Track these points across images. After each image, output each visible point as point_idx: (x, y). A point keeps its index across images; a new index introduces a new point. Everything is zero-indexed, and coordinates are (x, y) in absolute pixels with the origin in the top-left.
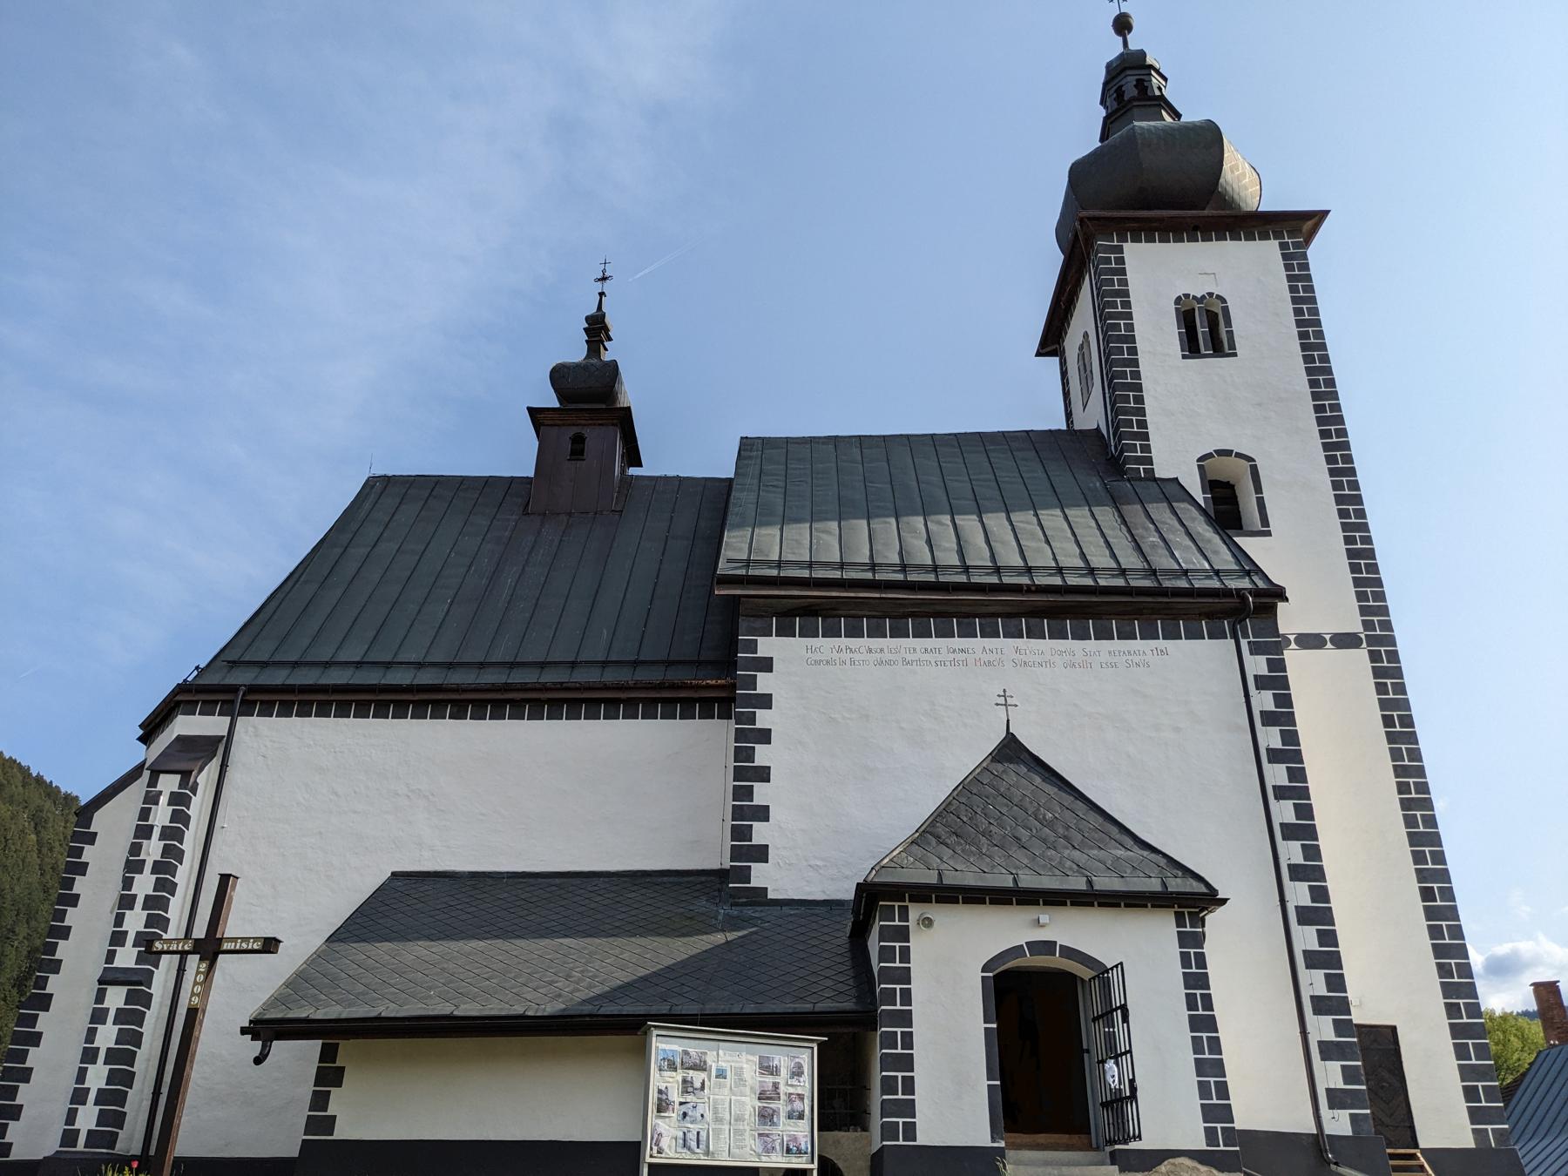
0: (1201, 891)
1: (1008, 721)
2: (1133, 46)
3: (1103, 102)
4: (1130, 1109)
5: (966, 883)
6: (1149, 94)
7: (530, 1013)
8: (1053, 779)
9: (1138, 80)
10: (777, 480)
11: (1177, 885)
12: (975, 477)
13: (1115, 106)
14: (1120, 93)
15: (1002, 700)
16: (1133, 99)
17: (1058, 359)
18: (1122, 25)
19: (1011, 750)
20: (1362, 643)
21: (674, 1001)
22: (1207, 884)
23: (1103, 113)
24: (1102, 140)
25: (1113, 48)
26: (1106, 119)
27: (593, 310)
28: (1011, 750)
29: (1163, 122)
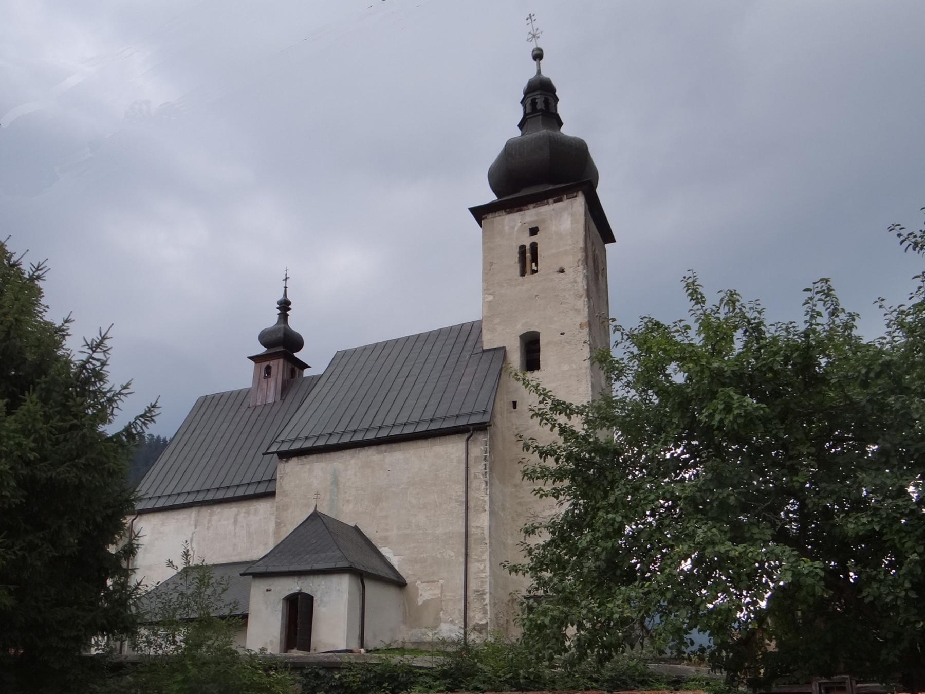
2: (545, 74)
18: (538, 56)
27: (541, 62)
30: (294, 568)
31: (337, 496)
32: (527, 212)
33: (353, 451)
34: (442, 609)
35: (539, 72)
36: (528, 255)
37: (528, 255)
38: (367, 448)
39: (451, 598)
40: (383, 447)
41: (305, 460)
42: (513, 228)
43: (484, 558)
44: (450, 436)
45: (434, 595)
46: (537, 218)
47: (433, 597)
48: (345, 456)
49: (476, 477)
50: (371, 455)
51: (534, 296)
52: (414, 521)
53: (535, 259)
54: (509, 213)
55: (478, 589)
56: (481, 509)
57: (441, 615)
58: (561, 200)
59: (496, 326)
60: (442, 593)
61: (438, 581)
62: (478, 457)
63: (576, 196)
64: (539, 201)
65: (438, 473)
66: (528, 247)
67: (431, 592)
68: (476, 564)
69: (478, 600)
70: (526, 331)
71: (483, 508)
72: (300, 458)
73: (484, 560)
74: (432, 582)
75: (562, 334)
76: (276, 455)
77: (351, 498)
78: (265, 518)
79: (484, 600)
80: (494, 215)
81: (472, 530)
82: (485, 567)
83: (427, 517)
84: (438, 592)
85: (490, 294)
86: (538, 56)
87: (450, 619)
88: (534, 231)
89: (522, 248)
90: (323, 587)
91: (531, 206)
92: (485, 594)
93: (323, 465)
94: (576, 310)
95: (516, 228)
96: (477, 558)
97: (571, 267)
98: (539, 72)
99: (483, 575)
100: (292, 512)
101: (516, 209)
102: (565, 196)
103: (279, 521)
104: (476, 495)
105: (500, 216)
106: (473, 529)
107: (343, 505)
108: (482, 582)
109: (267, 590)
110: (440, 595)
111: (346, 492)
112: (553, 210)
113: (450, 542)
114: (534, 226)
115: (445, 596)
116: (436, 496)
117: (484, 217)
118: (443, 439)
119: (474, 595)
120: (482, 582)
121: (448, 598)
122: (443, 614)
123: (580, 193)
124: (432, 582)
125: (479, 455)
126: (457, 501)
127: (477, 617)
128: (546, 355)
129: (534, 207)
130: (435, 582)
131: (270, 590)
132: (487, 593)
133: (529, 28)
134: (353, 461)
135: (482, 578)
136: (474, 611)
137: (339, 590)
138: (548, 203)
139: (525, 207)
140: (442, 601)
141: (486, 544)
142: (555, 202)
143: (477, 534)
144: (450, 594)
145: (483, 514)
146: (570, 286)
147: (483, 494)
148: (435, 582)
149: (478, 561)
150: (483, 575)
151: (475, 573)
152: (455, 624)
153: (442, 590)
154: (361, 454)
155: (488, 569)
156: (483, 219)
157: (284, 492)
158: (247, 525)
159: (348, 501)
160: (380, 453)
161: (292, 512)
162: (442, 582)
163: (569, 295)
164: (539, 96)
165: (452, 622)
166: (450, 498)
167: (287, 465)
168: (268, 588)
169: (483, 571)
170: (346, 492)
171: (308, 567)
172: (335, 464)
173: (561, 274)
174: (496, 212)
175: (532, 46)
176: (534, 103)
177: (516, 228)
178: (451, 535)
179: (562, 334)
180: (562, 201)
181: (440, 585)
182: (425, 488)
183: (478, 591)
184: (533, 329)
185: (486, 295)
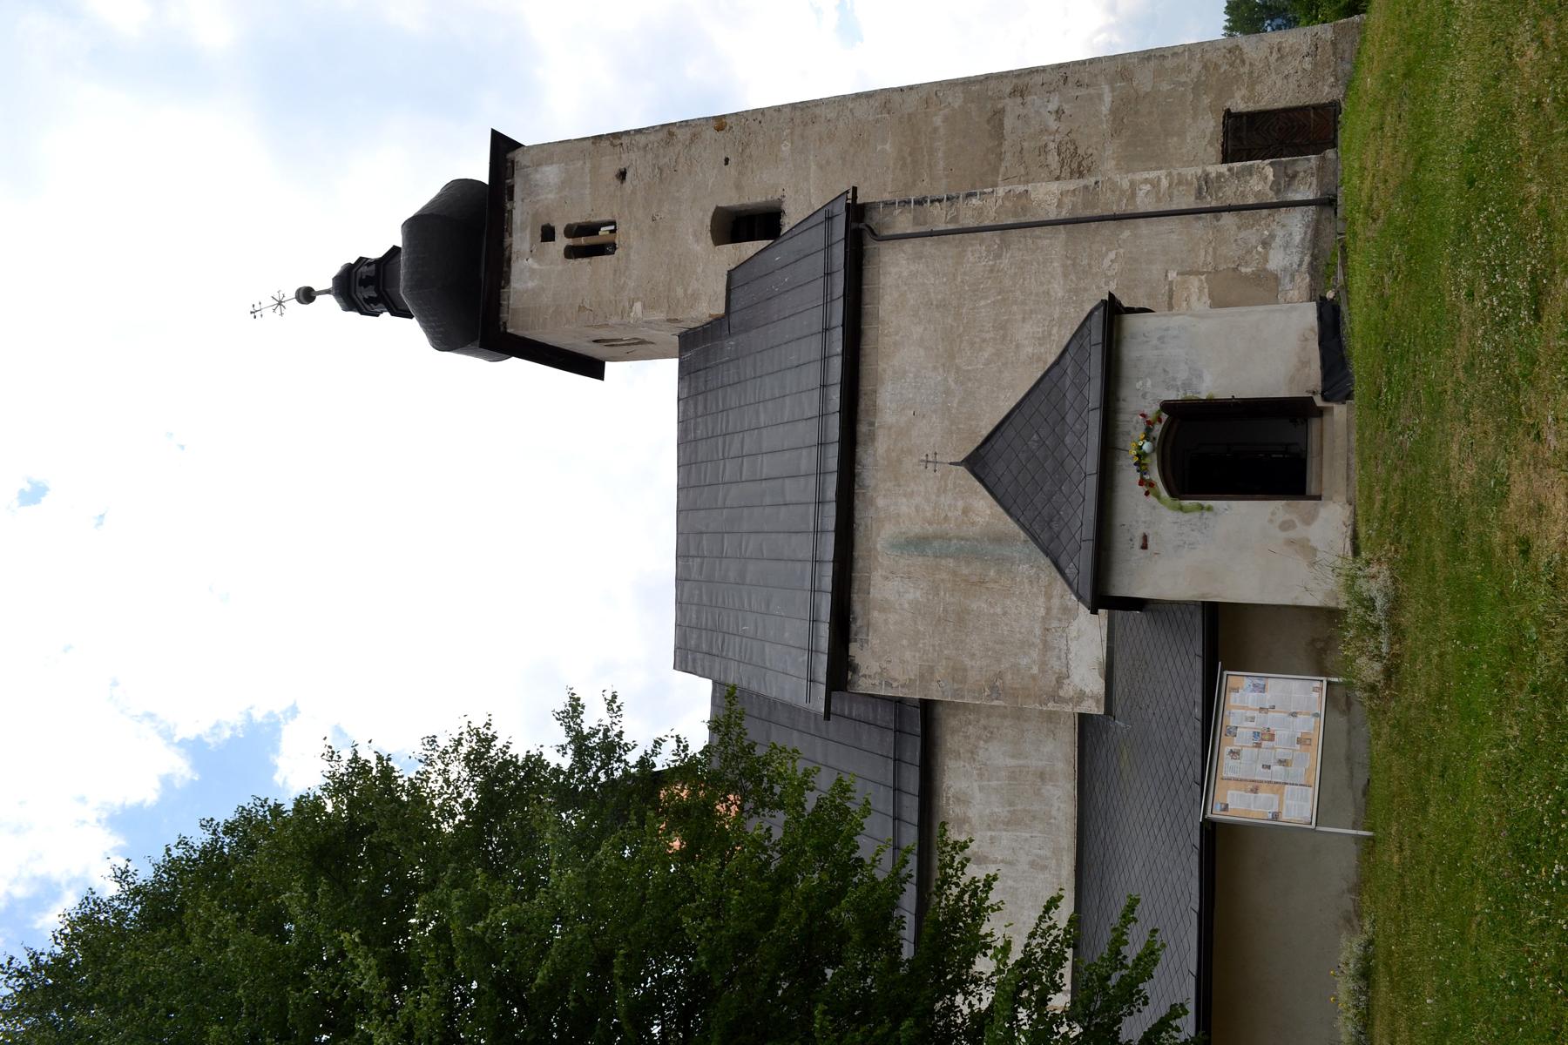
0: (1102, 314)
1: (951, 464)
2: (329, 285)
3: (377, 315)
4: (1314, 424)
5: (1092, 519)
6: (373, 274)
7: (1197, 909)
8: (1002, 430)
9: (360, 285)
10: (717, 640)
11: (1096, 335)
12: (720, 454)
13: (380, 305)
14: (370, 301)
15: (930, 466)
16: (377, 290)
17: (607, 363)
18: (307, 295)
19: (976, 463)
20: (1352, 683)
21: (1191, 779)
22: (1096, 308)
23: (386, 315)
24: (411, 317)
25: (328, 304)
26: (393, 314)
27: (316, 289)
28: (976, 463)
29: (403, 258)
30: (1091, 463)
31: (950, 540)
32: (515, 247)
33: (858, 503)
34: (1235, 270)
35: (327, 292)
36: (583, 241)
37: (583, 241)
38: (858, 469)
39: (1211, 250)
40: (863, 428)
41: (859, 623)
42: (532, 271)
43: (1125, 184)
44: (865, 281)
45: (1201, 290)
46: (529, 229)
47: (1206, 290)
48: (864, 516)
49: (954, 219)
50: (875, 456)
51: (653, 224)
52: (1030, 350)
53: (591, 229)
54: (508, 282)
55: (1193, 192)
56: (1024, 201)
57: (1249, 270)
58: (511, 189)
59: (689, 292)
60: (1198, 273)
61: (1171, 282)
62: (914, 218)
63: (513, 162)
64: (503, 225)
65: (934, 303)
66: (570, 242)
67: (1194, 298)
68: (1138, 200)
69: (1220, 188)
70: (709, 234)
71: (1020, 196)
72: (852, 636)
73: (1132, 184)
74: (1171, 297)
75: (727, 161)
76: (834, 693)
77: (960, 504)
78: (981, 775)
79: (1220, 175)
80: (504, 309)
81: (1064, 214)
82: (1146, 181)
83: (1024, 320)
84: (1194, 282)
85: (631, 307)
86: (307, 295)
87: (1260, 249)
88: (548, 234)
89: (572, 253)
90: (1149, 383)
91: (507, 241)
92: (1207, 175)
93: (877, 577)
94: (692, 141)
95: (536, 266)
96: (1125, 201)
97: (620, 158)
98: (327, 292)
99: (1165, 183)
100: (973, 656)
101: (505, 269)
102: (508, 181)
103: (988, 692)
104: (992, 214)
105: (509, 297)
106: (1064, 213)
107: (973, 524)
108: (1180, 183)
109: (1145, 547)
110: (1203, 277)
111: (946, 517)
112: (523, 200)
113: (1085, 262)
114: (539, 233)
115: (1205, 264)
116: (983, 303)
117: (502, 329)
118: (867, 298)
119: (1209, 198)
120: (1180, 183)
121: (1209, 259)
122: (1247, 264)
123: (510, 156)
124: (1171, 297)
125: (910, 217)
126: (998, 256)
127: (1256, 189)
128: (753, 195)
129: (511, 235)
130: (1171, 290)
131: (1145, 538)
132: (1204, 171)
133: (268, 312)
134: (881, 502)
135: (1170, 185)
136: (1243, 195)
137: (1161, 339)
138: (511, 212)
139: (507, 253)
140: (1216, 271)
141: (1096, 183)
142: (511, 199)
143: (1074, 206)
144: (1202, 253)
145: (1032, 196)
146: (650, 156)
147: (991, 201)
148: (1171, 290)
149: (1133, 195)
150: (1165, 183)
151: (1159, 200)
152: (1272, 236)
153: (1190, 273)
154: (867, 482)
155: (1152, 175)
156: (505, 328)
157: (922, 676)
158: (989, 828)
159: (965, 512)
160: (872, 437)
161: (973, 656)
162: (1172, 275)
163: (664, 156)
164: (359, 294)
165: (1266, 244)
166: (991, 271)
167: (863, 671)
168: (1138, 542)
169: (1155, 184)
170: (946, 517)
171: (1095, 419)
172: (879, 546)
173: (629, 175)
174: (500, 305)
175: (293, 306)
176: (370, 301)
177: (536, 266)
178: (1069, 262)
179: (727, 161)
180: (513, 186)
181: (1179, 278)
182: (961, 329)
183: (1200, 190)
184: (708, 221)
185: (632, 314)
